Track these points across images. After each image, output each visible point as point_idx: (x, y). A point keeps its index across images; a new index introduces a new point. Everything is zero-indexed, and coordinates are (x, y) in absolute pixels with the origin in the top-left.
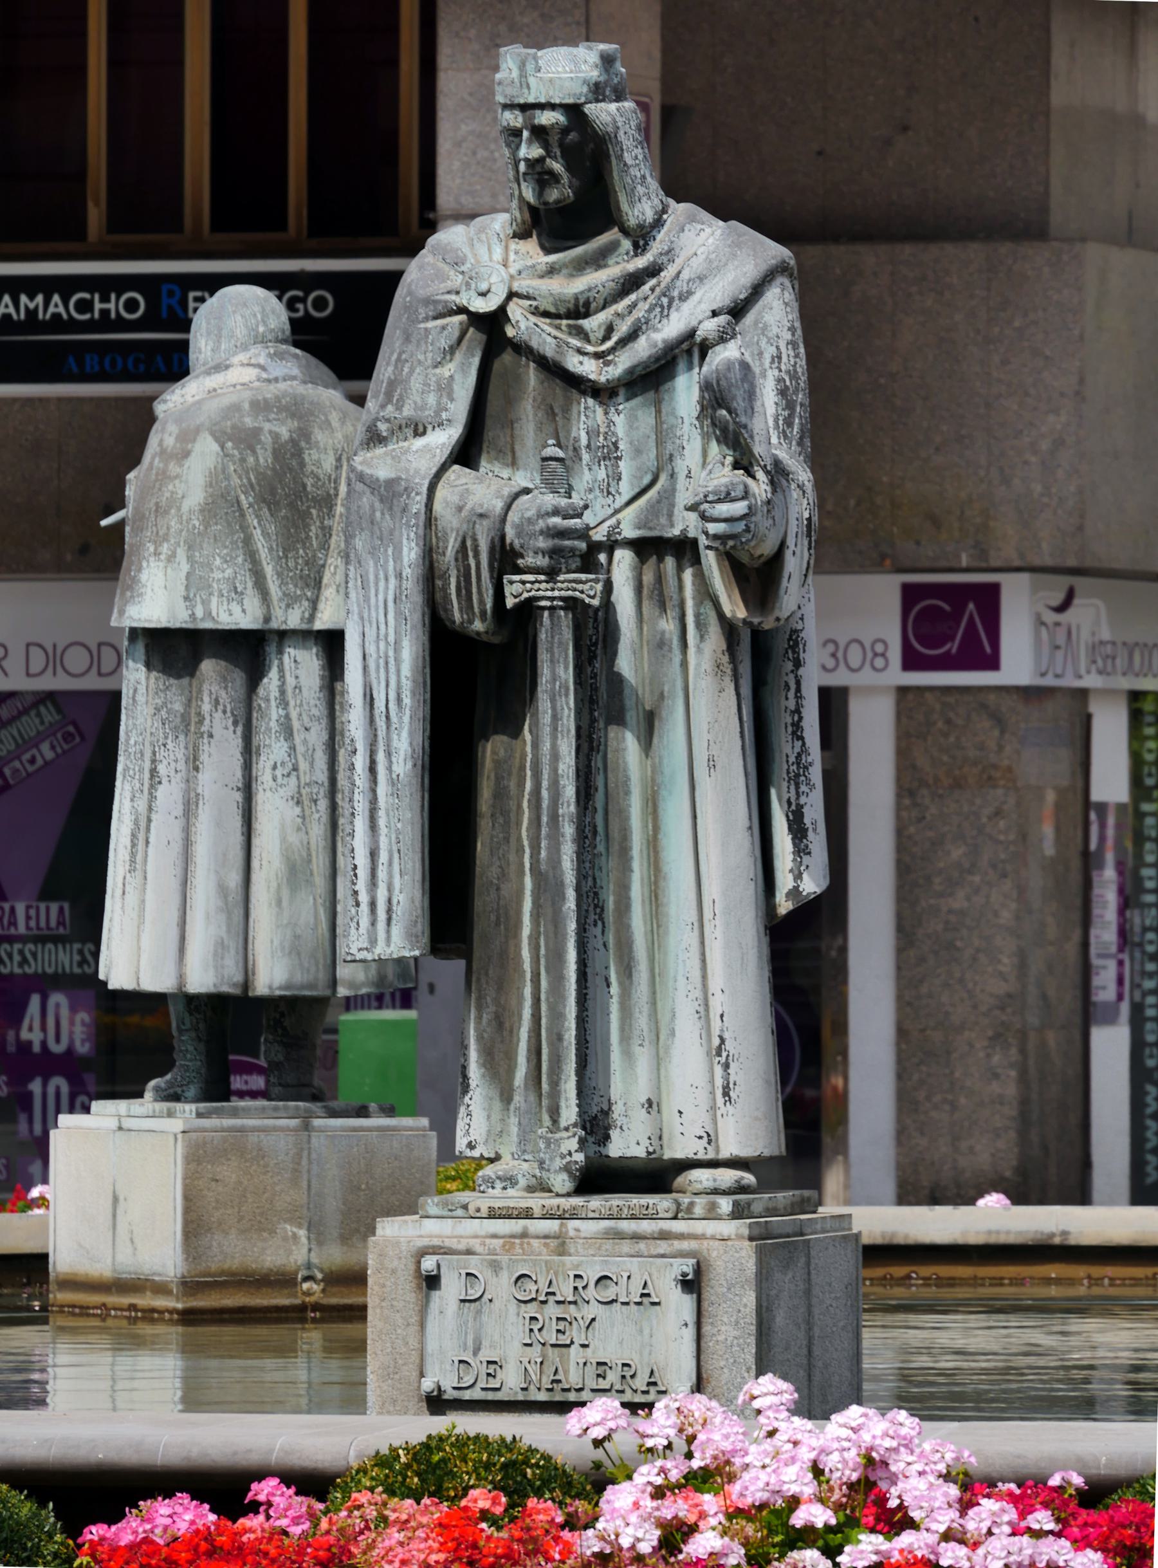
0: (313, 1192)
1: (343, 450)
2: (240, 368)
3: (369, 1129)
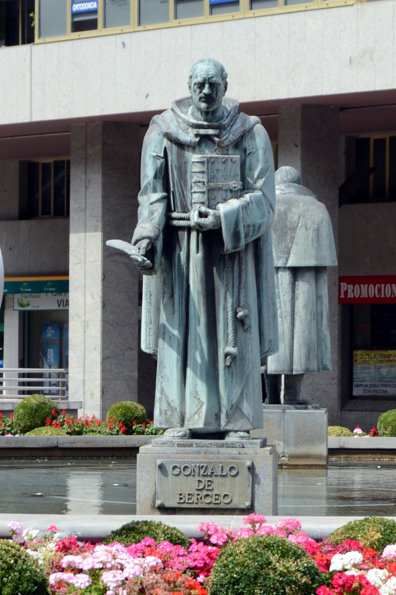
3: (305, 413)
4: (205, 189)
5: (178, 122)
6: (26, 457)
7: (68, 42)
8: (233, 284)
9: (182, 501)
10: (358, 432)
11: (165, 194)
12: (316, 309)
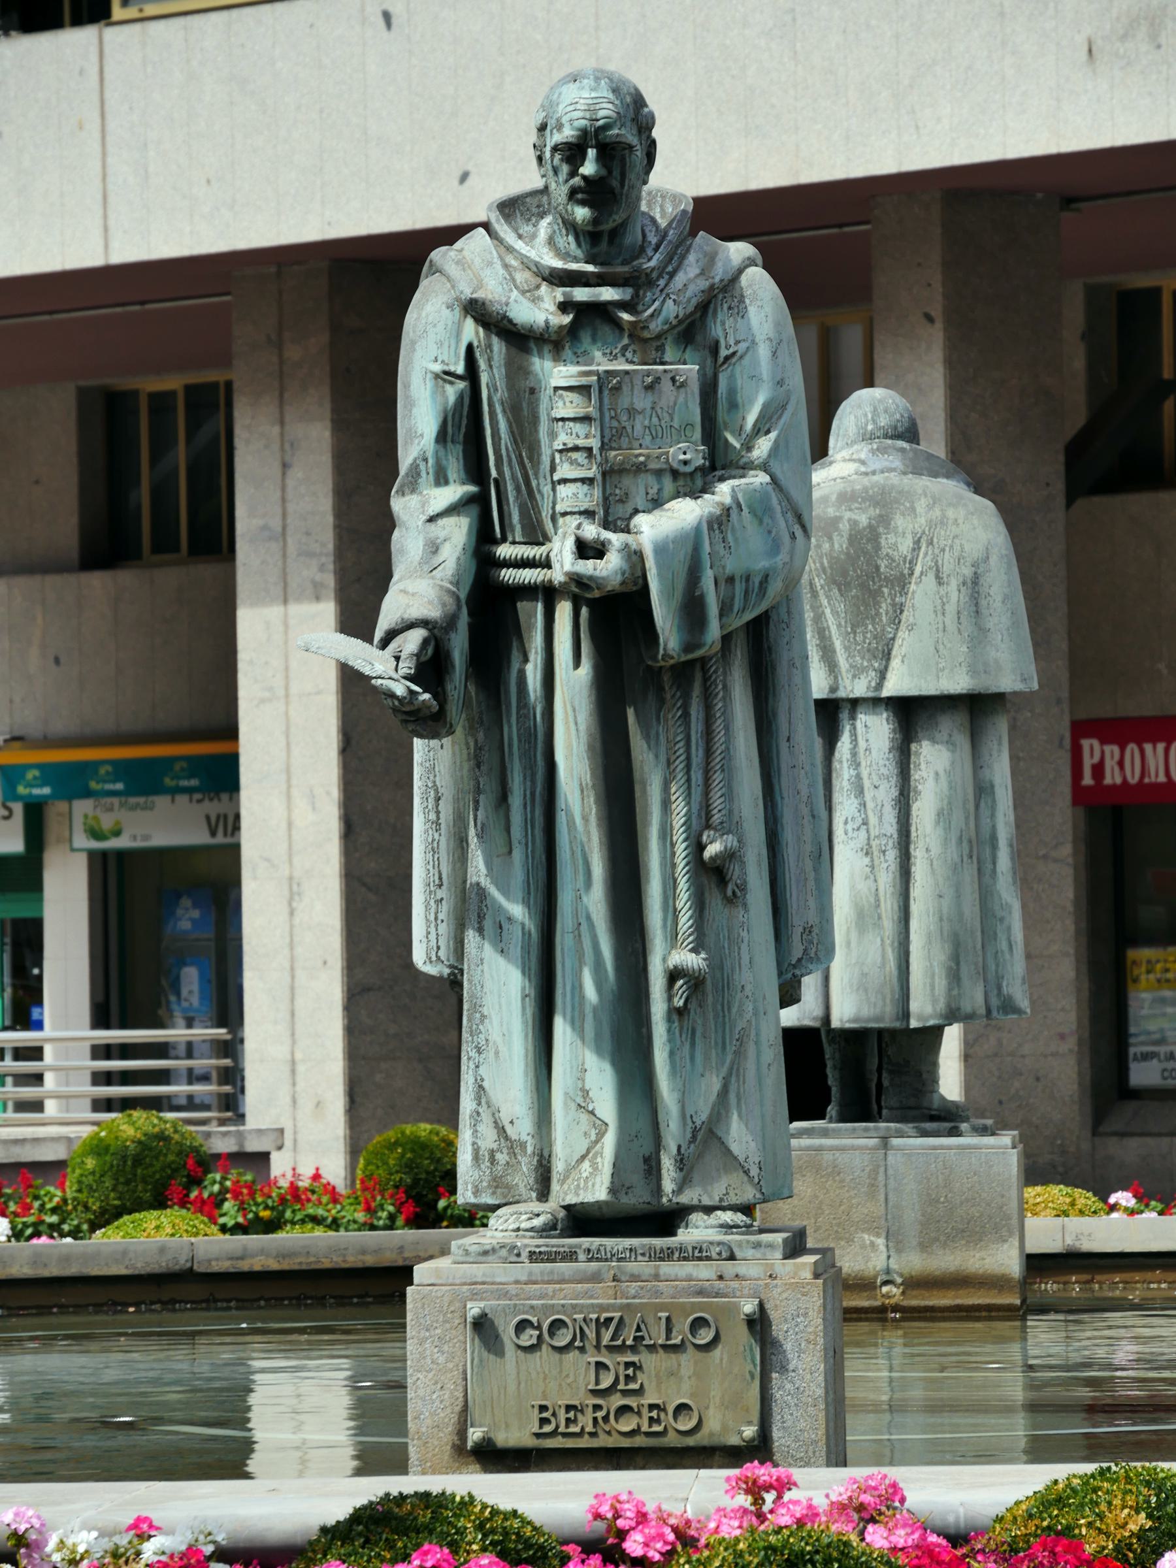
0: (891, 1204)
1: (924, 532)
2: (842, 464)
3: (949, 1148)
4: (592, 472)
5: (506, 266)
6: (94, 1305)
7: (214, 16)
8: (688, 758)
9: (547, 1429)
10: (1124, 1203)
11: (472, 489)
12: (977, 826)
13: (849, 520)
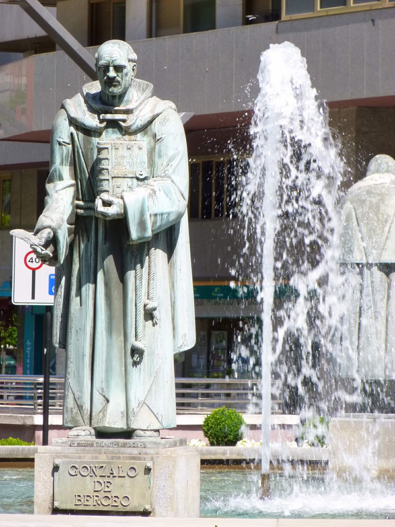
13: (369, 201)
